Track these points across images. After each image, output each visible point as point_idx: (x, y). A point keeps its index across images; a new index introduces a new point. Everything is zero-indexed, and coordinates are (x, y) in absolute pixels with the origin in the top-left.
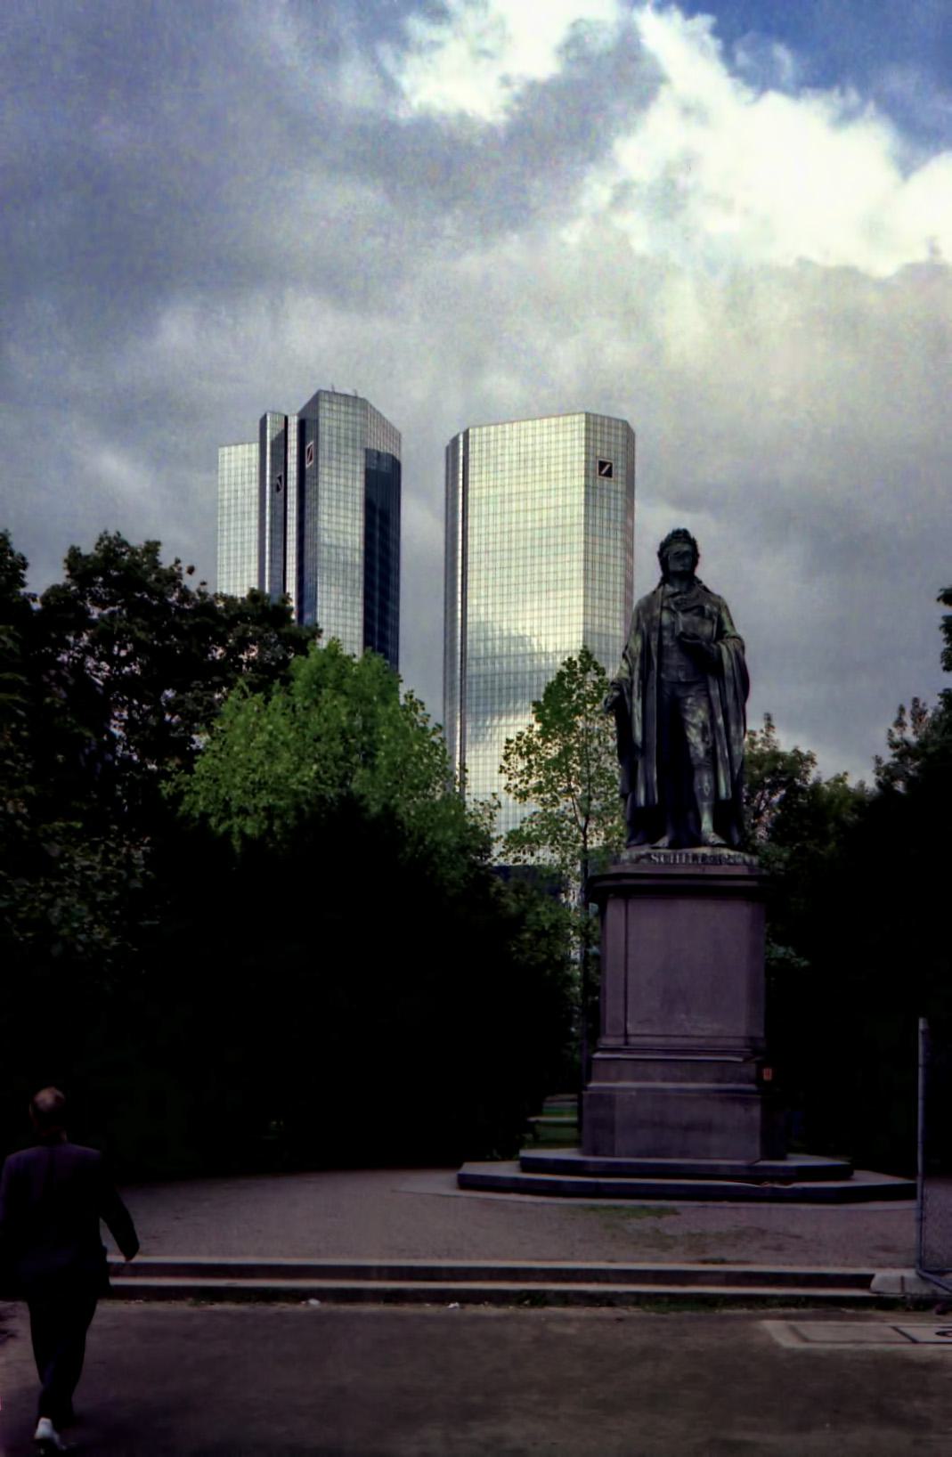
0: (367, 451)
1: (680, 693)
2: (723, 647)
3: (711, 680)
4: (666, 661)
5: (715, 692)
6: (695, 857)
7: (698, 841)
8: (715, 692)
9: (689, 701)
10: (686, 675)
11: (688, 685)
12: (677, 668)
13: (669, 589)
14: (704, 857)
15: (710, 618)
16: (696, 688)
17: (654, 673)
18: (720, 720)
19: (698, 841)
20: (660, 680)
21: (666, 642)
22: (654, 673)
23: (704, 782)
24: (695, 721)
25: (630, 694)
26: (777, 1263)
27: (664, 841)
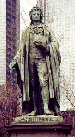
0: (35, 115)
1: (36, 62)
2: (50, 46)
3: (47, 57)
4: (31, 51)
5: (48, 61)
6: (40, 119)
7: (43, 113)
8: (48, 61)
9: (40, 64)
10: (38, 56)
11: (39, 59)
12: (35, 54)
13: (33, 26)
14: (43, 118)
15: (46, 36)
16: (42, 59)
17: (27, 55)
18: (50, 71)
19: (43, 113)
20: (29, 58)
21: (31, 45)
22: (27, 55)
23: (44, 92)
24: (41, 71)
25: (20, 62)
26: (28, 89)
27: (33, 113)
